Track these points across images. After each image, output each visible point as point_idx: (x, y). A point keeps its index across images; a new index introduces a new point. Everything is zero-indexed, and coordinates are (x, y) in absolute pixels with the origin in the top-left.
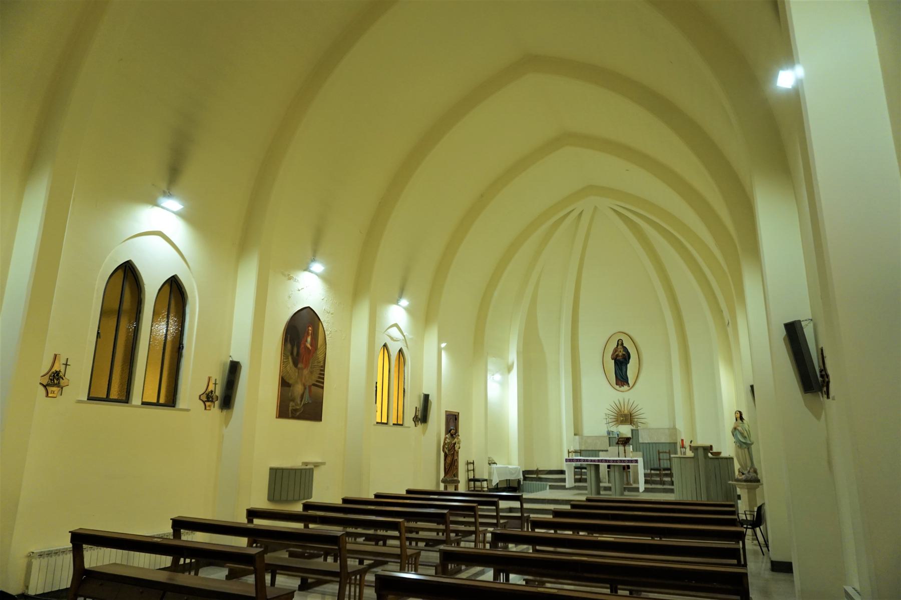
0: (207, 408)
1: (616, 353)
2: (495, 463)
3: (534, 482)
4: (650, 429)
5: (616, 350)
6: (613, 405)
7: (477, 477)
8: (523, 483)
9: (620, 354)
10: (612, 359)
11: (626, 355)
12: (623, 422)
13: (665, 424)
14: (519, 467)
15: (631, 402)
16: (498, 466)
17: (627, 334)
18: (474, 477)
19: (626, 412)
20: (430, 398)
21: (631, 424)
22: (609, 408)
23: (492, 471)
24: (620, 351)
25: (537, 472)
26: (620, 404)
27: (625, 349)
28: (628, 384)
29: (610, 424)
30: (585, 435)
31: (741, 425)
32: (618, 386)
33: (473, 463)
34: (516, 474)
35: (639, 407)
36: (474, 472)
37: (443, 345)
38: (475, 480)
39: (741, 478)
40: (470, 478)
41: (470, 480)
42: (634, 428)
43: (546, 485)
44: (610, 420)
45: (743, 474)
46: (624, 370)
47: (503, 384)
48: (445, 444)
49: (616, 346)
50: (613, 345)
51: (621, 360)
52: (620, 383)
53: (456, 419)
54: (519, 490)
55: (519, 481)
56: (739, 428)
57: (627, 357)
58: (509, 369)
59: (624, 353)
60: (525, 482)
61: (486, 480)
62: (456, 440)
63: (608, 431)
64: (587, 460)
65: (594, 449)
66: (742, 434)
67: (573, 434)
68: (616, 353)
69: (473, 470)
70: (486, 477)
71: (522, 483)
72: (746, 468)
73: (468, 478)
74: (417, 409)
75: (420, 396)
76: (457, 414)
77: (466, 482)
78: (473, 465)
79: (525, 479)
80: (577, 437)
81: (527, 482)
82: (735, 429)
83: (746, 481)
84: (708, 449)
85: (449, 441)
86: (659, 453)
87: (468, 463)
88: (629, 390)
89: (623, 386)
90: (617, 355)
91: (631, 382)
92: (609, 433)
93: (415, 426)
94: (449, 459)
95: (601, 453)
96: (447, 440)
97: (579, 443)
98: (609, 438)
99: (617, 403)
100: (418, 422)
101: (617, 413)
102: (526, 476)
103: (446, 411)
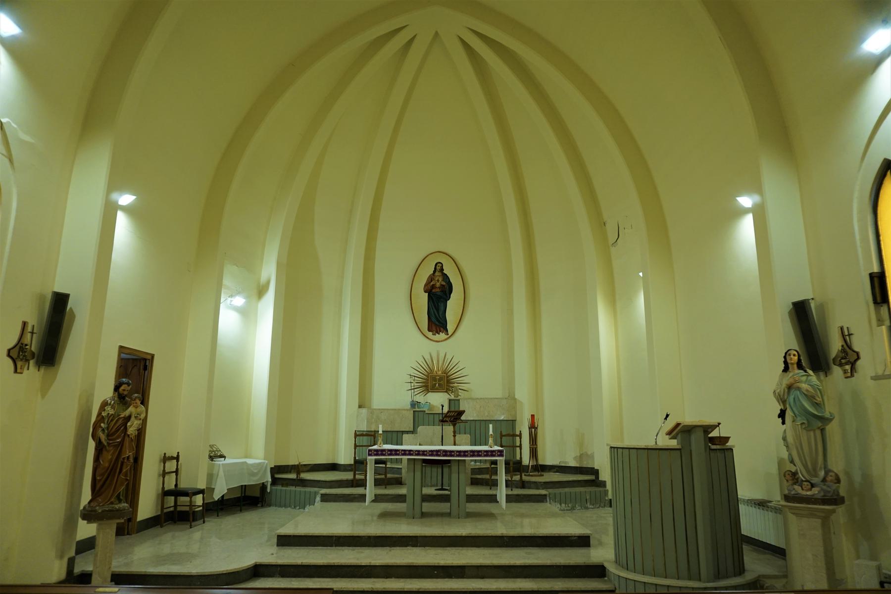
0: (19, 370)
1: (432, 283)
2: (222, 456)
3: (293, 488)
4: (478, 399)
5: (431, 278)
6: (421, 361)
7: (183, 485)
8: (271, 489)
9: (438, 285)
10: (425, 292)
11: (447, 287)
12: (434, 389)
13: (496, 391)
14: (266, 461)
15: (449, 357)
16: (228, 461)
17: (446, 254)
18: (176, 485)
19: (440, 373)
20: (70, 305)
21: (446, 392)
22: (415, 365)
23: (215, 472)
24: (438, 281)
25: (297, 469)
26: (432, 361)
27: (446, 277)
28: (447, 331)
29: (416, 390)
30: (374, 408)
31: (804, 378)
32: (431, 333)
33: (177, 458)
34: (260, 475)
35: (460, 366)
36: (177, 475)
37: (126, 199)
38: (177, 493)
39: (809, 493)
40: (166, 489)
41: (166, 493)
42: (452, 397)
43: (316, 493)
44: (416, 384)
45: (813, 486)
46: (442, 308)
47: (247, 314)
48: (100, 418)
49: (432, 272)
50: (428, 270)
51: (439, 293)
52: (434, 328)
53: (145, 368)
54: (262, 502)
55: (263, 487)
56: (804, 386)
57: (447, 290)
58: (261, 292)
59: (444, 283)
60: (273, 488)
61: (201, 492)
62: (131, 409)
63: (413, 401)
64: (396, 450)
65: (389, 429)
66: (810, 398)
67: (357, 406)
68: (432, 283)
69: (177, 472)
70: (202, 485)
71: (269, 491)
72: (815, 469)
73: (163, 488)
74: (29, 329)
75: (42, 297)
76: (149, 357)
77: (158, 495)
78: (178, 461)
79: (275, 481)
80: (364, 411)
81: (279, 488)
82: (790, 387)
83: (824, 501)
84: (707, 429)
85: (112, 412)
86: (502, 436)
87: (165, 459)
88: (446, 339)
89: (439, 334)
90: (433, 285)
91: (450, 327)
92: (414, 404)
93: (16, 371)
94: (108, 456)
95: (405, 436)
96: (108, 408)
97: (367, 419)
98: (414, 411)
99: (427, 357)
100: (27, 361)
101: (426, 373)
102: (277, 476)
103: (121, 348)
